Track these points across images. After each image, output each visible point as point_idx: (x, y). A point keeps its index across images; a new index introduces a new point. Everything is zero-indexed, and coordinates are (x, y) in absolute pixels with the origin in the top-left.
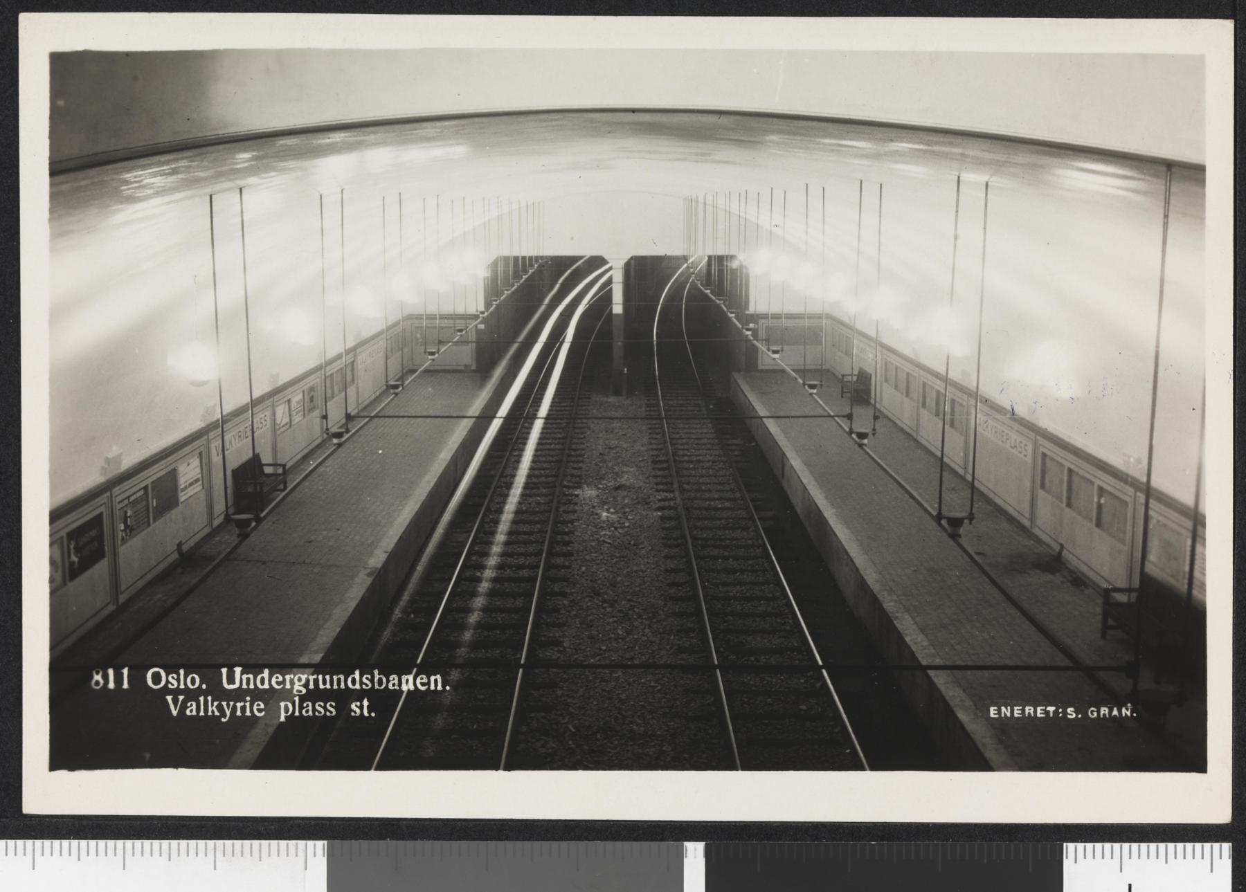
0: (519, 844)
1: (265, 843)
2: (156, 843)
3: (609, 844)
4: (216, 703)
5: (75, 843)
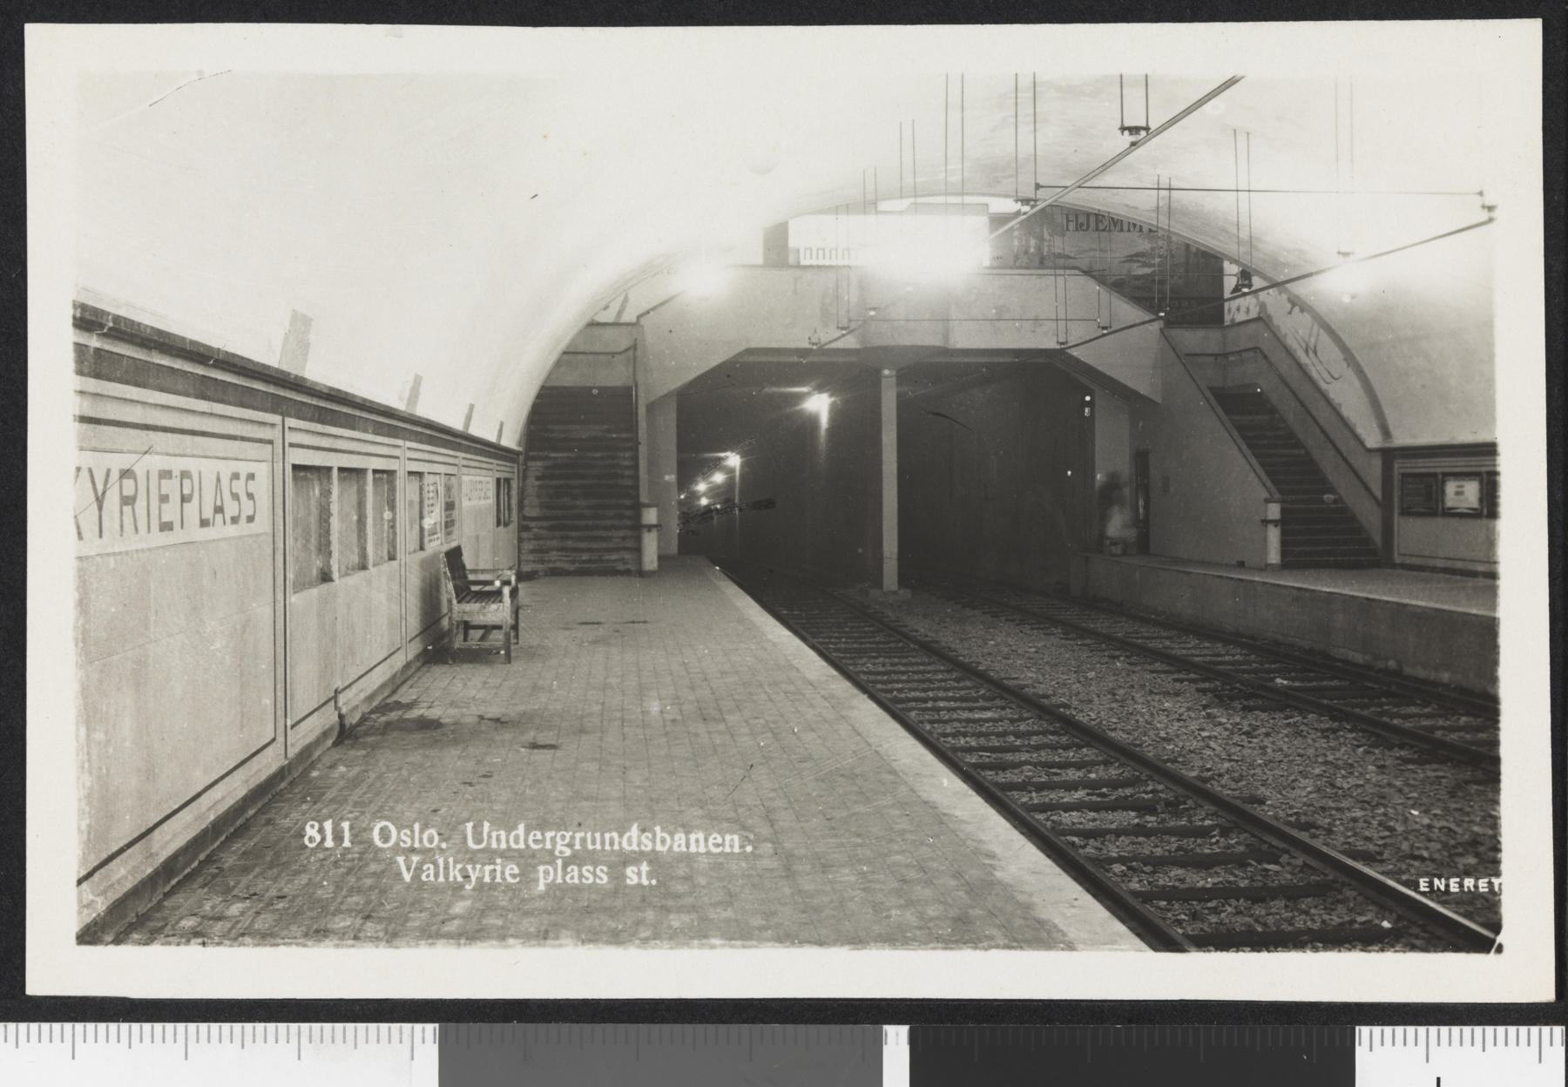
0: (677, 1028)
1: (361, 1026)
2: (226, 1026)
3: (790, 1027)
4: (459, 866)
5: (124, 1026)
